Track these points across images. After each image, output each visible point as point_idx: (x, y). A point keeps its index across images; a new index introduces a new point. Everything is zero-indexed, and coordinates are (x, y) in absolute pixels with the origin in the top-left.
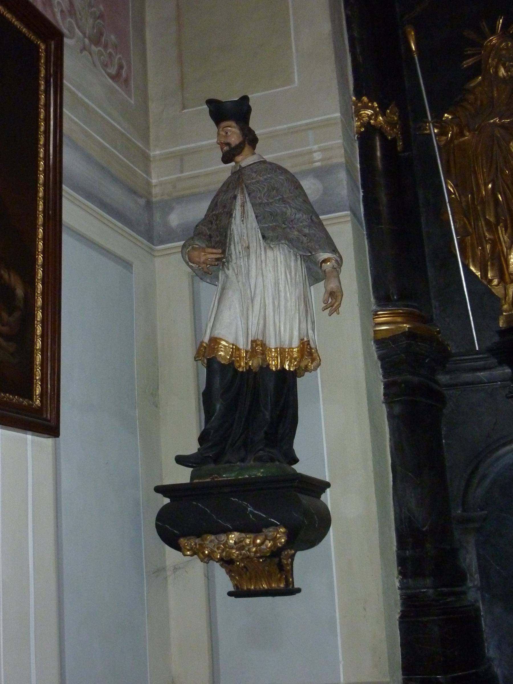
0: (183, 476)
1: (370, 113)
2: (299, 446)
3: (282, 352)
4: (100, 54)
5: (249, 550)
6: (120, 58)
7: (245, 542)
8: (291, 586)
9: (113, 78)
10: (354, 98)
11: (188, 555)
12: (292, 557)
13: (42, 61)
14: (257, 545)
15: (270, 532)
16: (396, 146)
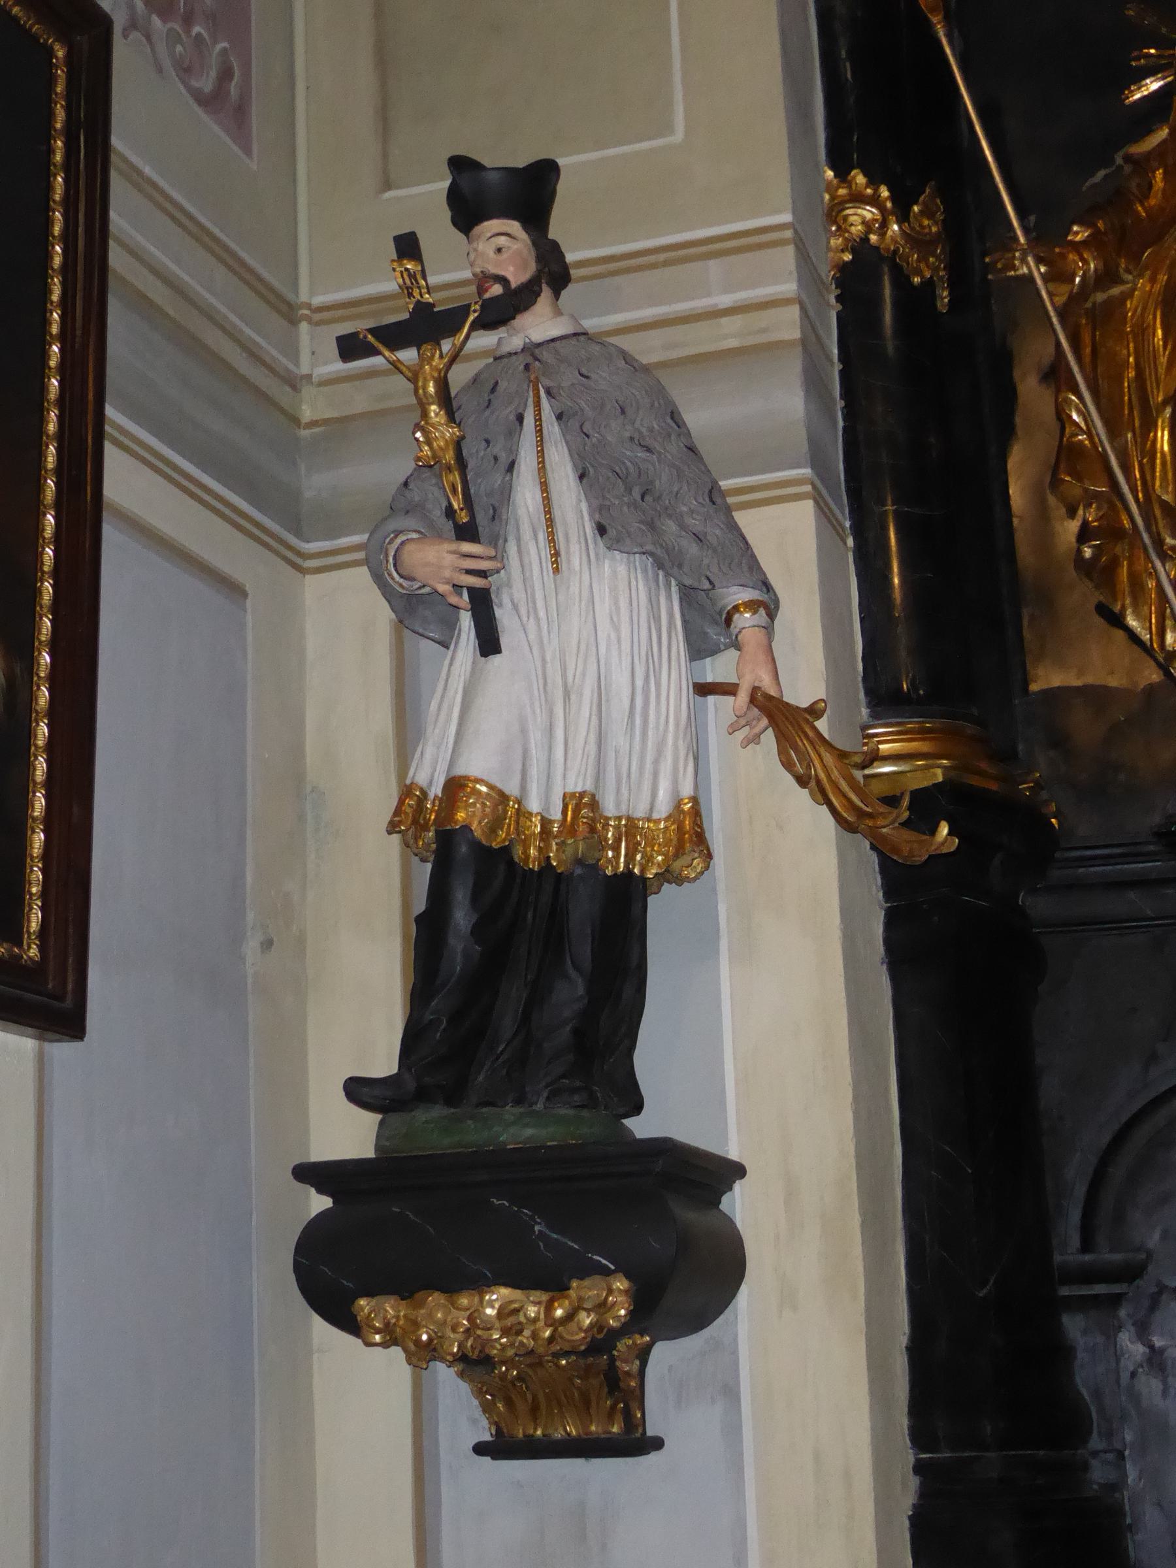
0: (350, 1135)
1: (869, 216)
2: (650, 1060)
3: (630, 829)
4: (173, 38)
5: (535, 1336)
6: (225, 50)
7: (525, 1315)
8: (640, 1430)
9: (204, 101)
10: (830, 174)
11: (376, 1345)
12: (644, 1355)
13: (59, 90)
14: (551, 1322)
15: (587, 1289)
16: (933, 297)
